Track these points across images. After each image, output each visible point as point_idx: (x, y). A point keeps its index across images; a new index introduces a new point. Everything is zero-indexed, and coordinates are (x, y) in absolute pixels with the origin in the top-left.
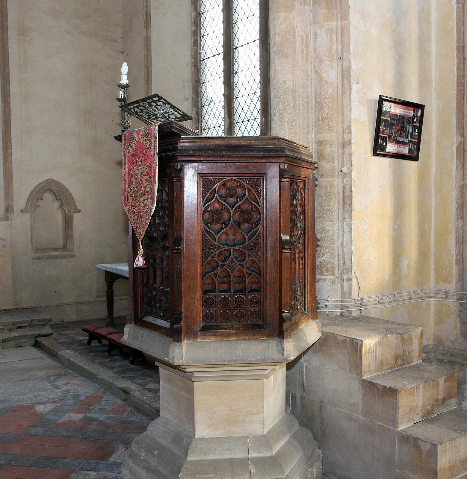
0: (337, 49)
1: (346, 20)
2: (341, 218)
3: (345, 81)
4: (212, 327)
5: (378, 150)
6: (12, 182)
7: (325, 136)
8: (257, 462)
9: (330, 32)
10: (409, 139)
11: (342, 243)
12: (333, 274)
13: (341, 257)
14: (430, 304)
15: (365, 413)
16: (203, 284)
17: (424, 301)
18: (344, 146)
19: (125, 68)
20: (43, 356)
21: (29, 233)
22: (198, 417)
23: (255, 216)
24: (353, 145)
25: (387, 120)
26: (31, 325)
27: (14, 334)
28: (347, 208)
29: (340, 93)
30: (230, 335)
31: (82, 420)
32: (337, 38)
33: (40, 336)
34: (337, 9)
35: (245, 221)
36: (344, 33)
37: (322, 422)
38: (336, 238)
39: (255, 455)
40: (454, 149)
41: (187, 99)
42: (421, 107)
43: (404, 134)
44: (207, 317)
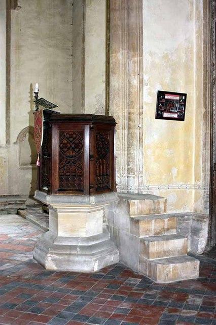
0: (137, 71)
1: (142, 56)
2: (138, 148)
3: (141, 85)
4: (62, 190)
5: (159, 116)
7: (132, 110)
11: (139, 160)
13: (138, 166)
14: (192, 192)
15: (131, 232)
16: (59, 174)
17: (188, 190)
19: (37, 86)
21: (18, 155)
23: (81, 145)
24: (144, 114)
25: (164, 103)
26: (16, 203)
27: (7, 207)
29: (138, 90)
30: (69, 193)
31: (27, 240)
32: (137, 65)
33: (20, 209)
34: (137, 51)
35: (76, 148)
36: (141, 62)
38: (136, 157)
42: (185, 95)
43: (174, 108)
44: (61, 185)
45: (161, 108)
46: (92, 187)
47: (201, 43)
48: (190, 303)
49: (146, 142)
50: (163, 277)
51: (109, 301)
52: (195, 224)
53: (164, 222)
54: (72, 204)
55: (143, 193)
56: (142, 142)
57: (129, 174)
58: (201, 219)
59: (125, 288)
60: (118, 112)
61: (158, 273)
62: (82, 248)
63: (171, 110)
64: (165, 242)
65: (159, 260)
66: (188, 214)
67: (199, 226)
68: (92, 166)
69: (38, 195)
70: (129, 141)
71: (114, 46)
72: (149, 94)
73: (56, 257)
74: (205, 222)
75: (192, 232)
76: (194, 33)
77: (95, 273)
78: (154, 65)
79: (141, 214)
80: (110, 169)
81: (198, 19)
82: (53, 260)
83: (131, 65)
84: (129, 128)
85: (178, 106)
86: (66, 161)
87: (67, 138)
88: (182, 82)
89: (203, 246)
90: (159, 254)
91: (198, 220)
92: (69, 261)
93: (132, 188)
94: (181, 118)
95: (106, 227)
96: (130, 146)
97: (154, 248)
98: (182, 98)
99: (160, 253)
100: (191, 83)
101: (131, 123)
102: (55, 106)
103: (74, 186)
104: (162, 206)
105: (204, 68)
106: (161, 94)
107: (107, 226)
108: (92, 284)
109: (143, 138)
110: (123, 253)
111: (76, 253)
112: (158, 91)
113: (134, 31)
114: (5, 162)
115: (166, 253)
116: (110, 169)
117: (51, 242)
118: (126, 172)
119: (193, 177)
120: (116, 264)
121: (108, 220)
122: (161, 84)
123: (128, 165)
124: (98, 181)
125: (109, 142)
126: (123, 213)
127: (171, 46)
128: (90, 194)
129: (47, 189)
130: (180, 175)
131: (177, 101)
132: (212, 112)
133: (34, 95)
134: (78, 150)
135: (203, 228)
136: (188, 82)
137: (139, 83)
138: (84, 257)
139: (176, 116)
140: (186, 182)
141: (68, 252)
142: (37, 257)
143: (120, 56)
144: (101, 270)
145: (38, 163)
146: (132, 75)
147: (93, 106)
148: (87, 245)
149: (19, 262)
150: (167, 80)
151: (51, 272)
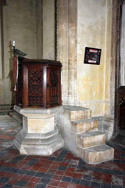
2: (74, 80)
3: (76, 43)
4: (30, 106)
5: (86, 62)
6: (4, 70)
7: (70, 59)
8: (41, 140)
9: (72, 30)
10: (96, 59)
12: (72, 95)
16: (28, 95)
18: (75, 61)
19: (14, 42)
20: (10, 117)
22: (29, 128)
23: (41, 79)
28: (76, 78)
30: (34, 107)
33: (9, 112)
35: (38, 80)
36: (76, 30)
37: (64, 133)
39: (41, 138)
40: (110, 61)
41: (53, 47)
42: (101, 50)
43: (94, 58)
44: (29, 103)
45: (87, 57)
46: (49, 104)
47: (110, 19)
48: (115, 184)
49: (78, 77)
50: (93, 160)
51: (61, 183)
52: (105, 123)
53: (91, 124)
54: (36, 114)
55: (77, 106)
56: (76, 77)
57: (69, 95)
58: (110, 120)
59: (70, 169)
60: (62, 58)
61: (90, 158)
62: (42, 140)
63: (92, 59)
64: (92, 137)
65: (90, 148)
66: (101, 117)
67: (108, 124)
68: (48, 91)
69: (16, 108)
70: (69, 76)
71: (60, 20)
72: (81, 49)
73: (26, 146)
74: (112, 122)
75: (104, 128)
76: (106, 13)
77: (51, 156)
78: (83, 32)
79: (77, 119)
80: (59, 93)
81: (109, 5)
82: (24, 148)
83: (70, 32)
84: (69, 69)
85: (97, 56)
86: (32, 88)
87: (36, 80)
88: (99, 43)
89: (111, 136)
90: (89, 144)
91: (107, 121)
92: (34, 149)
93: (71, 103)
94: (98, 63)
95: (56, 125)
96: (69, 79)
97: (86, 141)
98: (99, 52)
99: (90, 144)
100: (104, 45)
101: (70, 66)
102: (26, 55)
103: (38, 103)
104: (89, 114)
105: (112, 34)
106: (87, 49)
107: (57, 125)
108: (48, 166)
109: (77, 75)
110: (66, 142)
111: (38, 143)
112: (86, 47)
113: (72, 11)
114: (2, 87)
115: (94, 143)
116: (59, 93)
117: (24, 137)
118: (67, 93)
119: (104, 97)
120: (62, 148)
121: (57, 121)
122: (87, 43)
123: (68, 90)
124: (52, 99)
125: (58, 77)
126: (66, 118)
127: (88, 26)
128: (47, 108)
129: (21, 105)
130: (97, 95)
131: (96, 53)
132: (117, 59)
133: (13, 48)
134: (39, 81)
135: (111, 125)
136: (102, 43)
137: (74, 42)
138: (43, 146)
139: (95, 62)
140: (100, 99)
141: (34, 143)
142: (15, 145)
143: (63, 27)
144: (53, 153)
145: (15, 89)
146: (71, 37)
147: (48, 55)
148: (45, 138)
149: (4, 148)
150: (91, 41)
151: (24, 156)
